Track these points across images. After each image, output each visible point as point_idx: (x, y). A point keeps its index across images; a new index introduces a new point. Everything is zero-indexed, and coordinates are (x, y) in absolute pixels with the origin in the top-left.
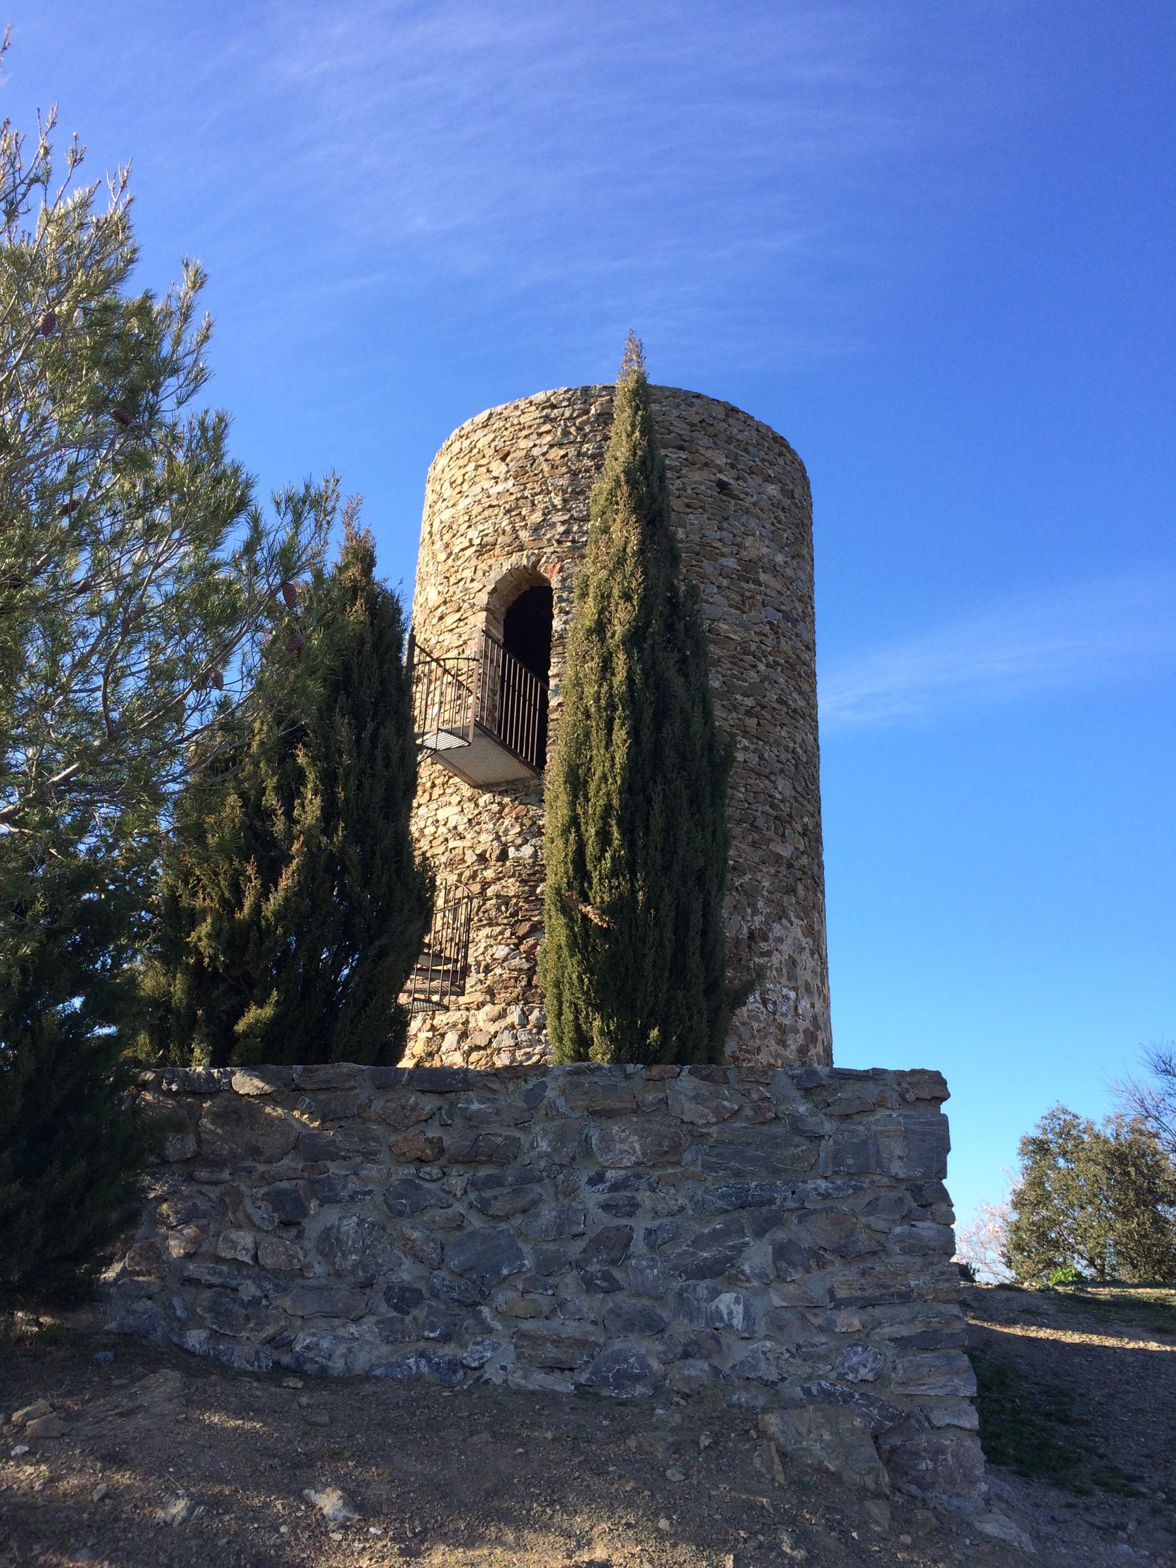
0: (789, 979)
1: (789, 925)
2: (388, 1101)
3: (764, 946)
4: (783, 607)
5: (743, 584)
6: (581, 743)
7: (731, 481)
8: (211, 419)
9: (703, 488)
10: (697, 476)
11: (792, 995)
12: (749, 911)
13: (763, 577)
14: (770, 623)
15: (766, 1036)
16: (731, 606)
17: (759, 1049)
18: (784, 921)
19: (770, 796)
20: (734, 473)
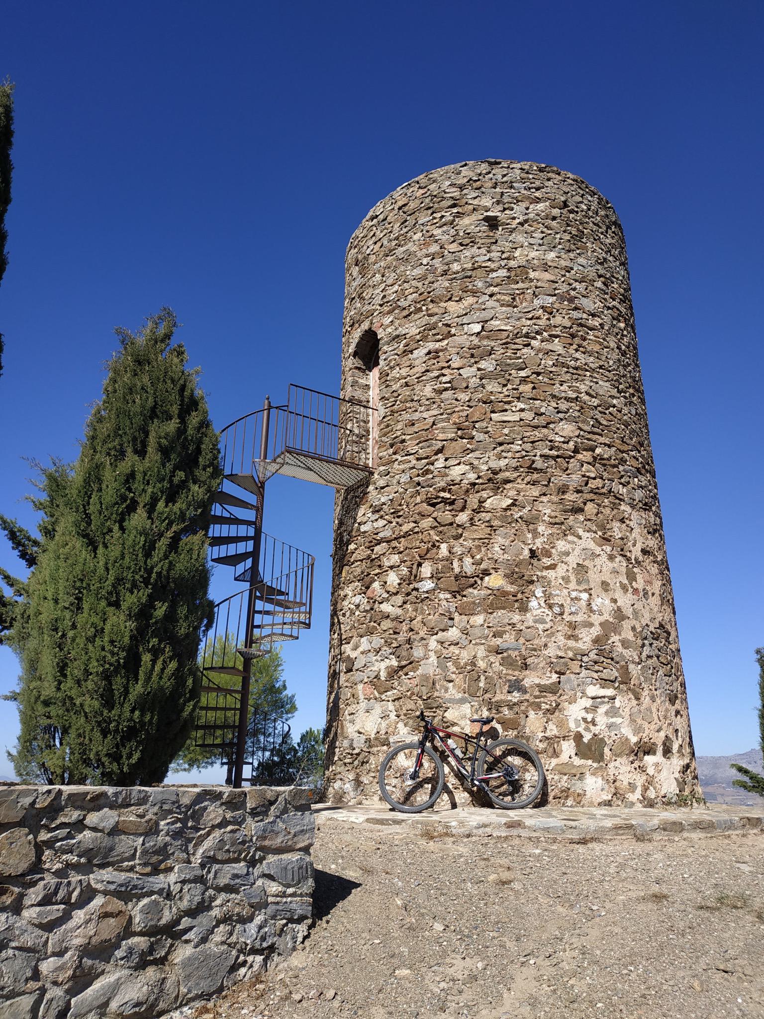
0: (579, 582)
1: (576, 539)
2: (155, 845)
3: (547, 561)
4: (557, 292)
5: (513, 286)
6: (507, 228)
7: (499, 214)
8: (308, 730)
9: (473, 227)
10: (466, 221)
11: (585, 596)
12: (530, 536)
13: (532, 275)
14: (542, 307)
15: (553, 634)
16: (502, 305)
17: (546, 645)
18: (570, 538)
19: (551, 441)
20: (500, 207)
